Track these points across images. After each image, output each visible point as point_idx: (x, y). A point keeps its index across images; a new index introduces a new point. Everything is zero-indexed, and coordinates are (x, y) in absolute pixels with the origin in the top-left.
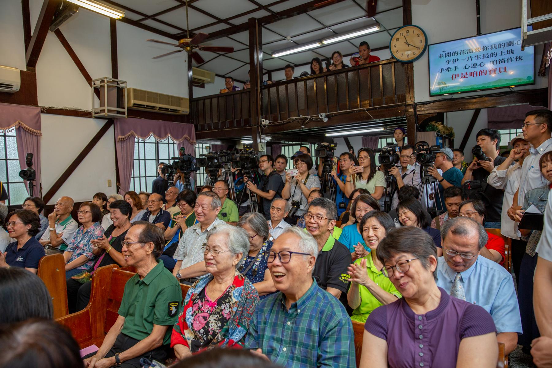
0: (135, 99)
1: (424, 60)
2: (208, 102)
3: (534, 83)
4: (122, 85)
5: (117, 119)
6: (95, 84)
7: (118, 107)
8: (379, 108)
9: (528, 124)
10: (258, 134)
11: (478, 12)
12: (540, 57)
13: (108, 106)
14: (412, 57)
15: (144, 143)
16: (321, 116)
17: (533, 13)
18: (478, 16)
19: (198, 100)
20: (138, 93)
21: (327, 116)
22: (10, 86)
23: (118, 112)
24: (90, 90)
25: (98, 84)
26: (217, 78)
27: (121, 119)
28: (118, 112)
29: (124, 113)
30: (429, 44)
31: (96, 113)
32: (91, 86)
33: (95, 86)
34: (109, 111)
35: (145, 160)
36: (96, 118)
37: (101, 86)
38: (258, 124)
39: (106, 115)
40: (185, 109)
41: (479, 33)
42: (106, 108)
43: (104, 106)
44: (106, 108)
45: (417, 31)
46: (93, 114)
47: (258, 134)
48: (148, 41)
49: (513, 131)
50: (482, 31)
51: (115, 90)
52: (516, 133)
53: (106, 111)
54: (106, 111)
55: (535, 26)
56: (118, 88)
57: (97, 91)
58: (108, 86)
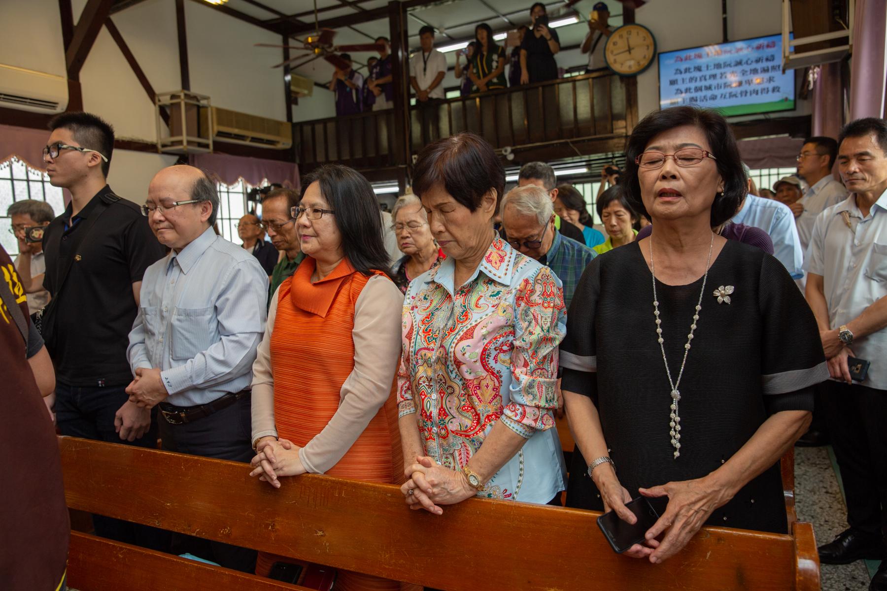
0: (220, 123)
1: (652, 72)
2: (319, 128)
3: (794, 109)
4: (203, 102)
5: (193, 156)
6: (159, 101)
7: (199, 136)
8: (589, 140)
9: (807, 153)
10: (406, 179)
11: (725, 11)
12: (800, 81)
13: (188, 134)
14: (634, 69)
15: (228, 192)
16: (506, 151)
17: (796, 33)
18: (724, 16)
19: (301, 124)
20: (223, 115)
21: (513, 152)
22: (53, 105)
23: (200, 145)
24: (152, 110)
25: (166, 100)
26: (316, 89)
27: (201, 155)
28: (200, 145)
29: (207, 146)
30: (658, 51)
31: (164, 146)
32: (154, 103)
33: (160, 103)
34: (189, 143)
35: (230, 219)
36: (164, 153)
37: (172, 104)
38: (405, 163)
39: (185, 150)
40: (285, 143)
41: (726, 40)
42: (184, 138)
43: (181, 134)
44: (184, 138)
45: (643, 33)
46: (159, 147)
47: (406, 179)
48: (425, 74)
49: (774, 171)
50: (729, 37)
51: (195, 110)
52: (778, 174)
53: (185, 143)
54: (185, 143)
55: (798, 49)
56: (199, 107)
57: (165, 113)
58: (186, 104)
